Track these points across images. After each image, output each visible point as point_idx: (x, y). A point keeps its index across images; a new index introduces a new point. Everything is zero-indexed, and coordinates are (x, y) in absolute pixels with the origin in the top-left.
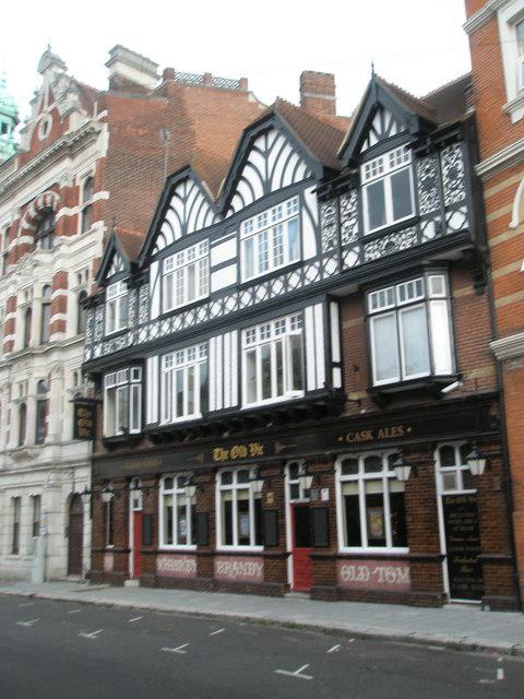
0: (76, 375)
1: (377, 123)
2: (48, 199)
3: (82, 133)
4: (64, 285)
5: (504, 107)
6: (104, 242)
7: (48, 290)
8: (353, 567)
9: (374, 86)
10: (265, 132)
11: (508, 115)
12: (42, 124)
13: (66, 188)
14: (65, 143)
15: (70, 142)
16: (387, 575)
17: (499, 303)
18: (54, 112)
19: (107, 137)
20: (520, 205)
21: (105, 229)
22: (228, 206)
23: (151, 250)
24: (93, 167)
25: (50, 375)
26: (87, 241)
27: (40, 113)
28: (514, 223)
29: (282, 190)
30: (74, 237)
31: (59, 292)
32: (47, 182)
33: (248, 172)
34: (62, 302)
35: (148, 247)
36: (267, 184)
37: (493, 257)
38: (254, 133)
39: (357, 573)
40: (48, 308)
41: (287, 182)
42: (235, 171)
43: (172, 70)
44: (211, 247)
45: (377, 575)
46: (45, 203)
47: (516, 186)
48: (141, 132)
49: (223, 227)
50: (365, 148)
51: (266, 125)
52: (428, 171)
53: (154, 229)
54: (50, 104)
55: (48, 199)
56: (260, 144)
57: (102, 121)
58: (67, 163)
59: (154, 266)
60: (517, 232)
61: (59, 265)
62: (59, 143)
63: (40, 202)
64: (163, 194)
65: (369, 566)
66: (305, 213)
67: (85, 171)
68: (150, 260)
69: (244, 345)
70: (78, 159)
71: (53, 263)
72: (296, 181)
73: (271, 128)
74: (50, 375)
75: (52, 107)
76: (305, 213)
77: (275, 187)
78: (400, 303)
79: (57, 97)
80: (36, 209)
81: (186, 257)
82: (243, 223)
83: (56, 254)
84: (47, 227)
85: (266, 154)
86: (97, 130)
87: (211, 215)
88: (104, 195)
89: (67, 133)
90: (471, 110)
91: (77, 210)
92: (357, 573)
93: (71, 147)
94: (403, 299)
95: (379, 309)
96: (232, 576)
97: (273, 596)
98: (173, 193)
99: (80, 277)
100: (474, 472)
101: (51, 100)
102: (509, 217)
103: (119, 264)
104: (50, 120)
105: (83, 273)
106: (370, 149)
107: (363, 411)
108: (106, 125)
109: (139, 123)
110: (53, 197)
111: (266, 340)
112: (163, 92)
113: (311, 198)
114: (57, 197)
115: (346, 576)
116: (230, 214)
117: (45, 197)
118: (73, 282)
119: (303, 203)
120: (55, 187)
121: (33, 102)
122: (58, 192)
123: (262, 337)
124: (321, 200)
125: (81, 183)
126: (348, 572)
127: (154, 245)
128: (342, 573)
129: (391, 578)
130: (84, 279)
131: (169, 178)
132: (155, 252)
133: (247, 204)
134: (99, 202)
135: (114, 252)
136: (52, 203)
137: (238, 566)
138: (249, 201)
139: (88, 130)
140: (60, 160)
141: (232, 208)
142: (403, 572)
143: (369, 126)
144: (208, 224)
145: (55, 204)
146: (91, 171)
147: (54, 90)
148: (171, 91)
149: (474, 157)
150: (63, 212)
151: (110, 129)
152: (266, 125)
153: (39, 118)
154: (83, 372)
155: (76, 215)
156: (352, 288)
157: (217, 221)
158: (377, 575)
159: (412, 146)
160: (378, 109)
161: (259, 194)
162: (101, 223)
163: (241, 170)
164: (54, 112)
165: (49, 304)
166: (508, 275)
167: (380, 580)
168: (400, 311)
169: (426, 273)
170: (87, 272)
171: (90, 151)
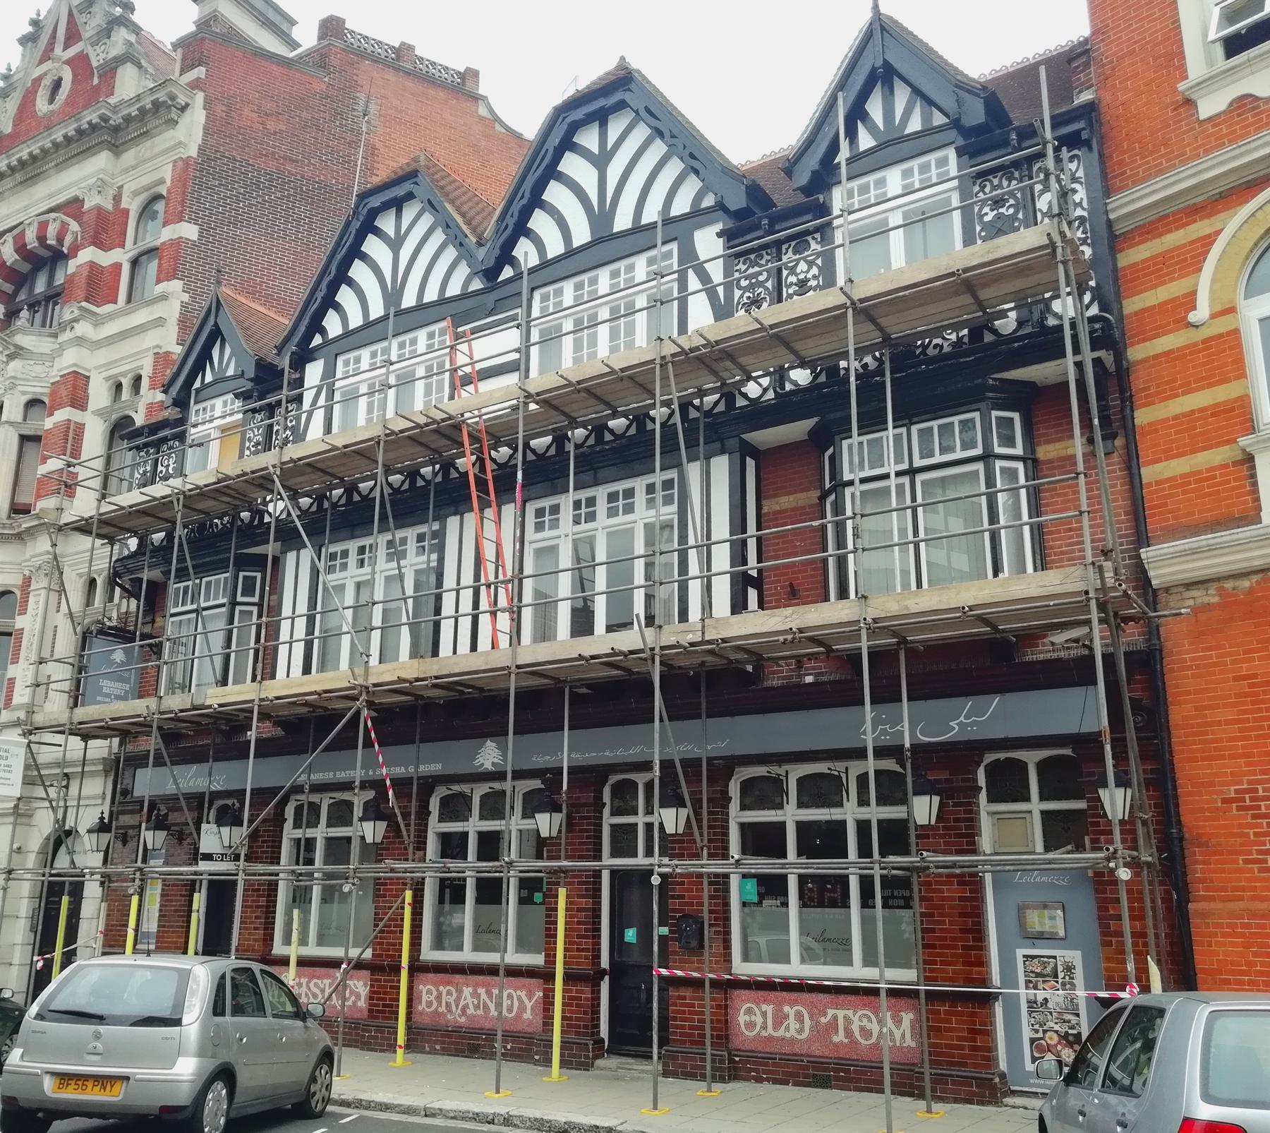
0: (92, 583)
1: (875, 108)
2: (52, 231)
3: (147, 102)
4: (79, 401)
5: (1182, 86)
6: (183, 322)
7: (35, 411)
8: (769, 1009)
9: (877, 27)
10: (397, 205)
11: (1189, 103)
12: (47, 82)
13: (99, 210)
14: (104, 119)
15: (116, 119)
16: (855, 1028)
17: (1149, 473)
18: (80, 64)
19: (203, 120)
20: (1214, 280)
21: (186, 297)
22: (506, 257)
23: (308, 337)
24: (167, 173)
25: (27, 581)
26: (141, 316)
27: (40, 63)
28: (1201, 313)
29: (420, 307)
30: (109, 308)
31: (62, 415)
32: (51, 196)
33: (555, 193)
34: (72, 438)
35: (302, 328)
36: (392, 295)
37: (1138, 381)
38: (375, 202)
39: (780, 1020)
40: (30, 448)
41: (431, 295)
42: (528, 186)
43: (341, 22)
44: (457, 337)
45: (833, 1025)
46: (42, 238)
47: (1207, 242)
48: (272, 125)
49: (491, 298)
50: (197, 384)
51: (400, 191)
52: (998, 203)
53: (320, 295)
54: (67, 46)
55: (52, 231)
56: (589, 139)
57: (196, 85)
58: (101, 161)
59: (314, 372)
60: (1206, 333)
61: (71, 359)
62: (91, 116)
63: (31, 238)
64: (348, 224)
65: (811, 1007)
66: (694, 282)
67: (146, 180)
68: (302, 358)
69: (530, 534)
70: (129, 157)
71: (53, 356)
72: (449, 294)
73: (410, 196)
74: (27, 581)
75: (71, 52)
76: (694, 282)
77: (409, 300)
78: (203, 605)
79: (88, 32)
80: (21, 248)
81: (421, 346)
82: (537, 295)
83: (66, 336)
84: (40, 287)
85: (395, 245)
86: (182, 100)
87: (463, 271)
88: (189, 231)
89: (112, 100)
90: (1086, 97)
91: (120, 256)
92: (780, 1020)
93: (117, 129)
94: (207, 599)
95: (180, 609)
96: (456, 1018)
97: (824, 1087)
98: (369, 227)
99: (119, 386)
100: (545, 833)
101: (73, 36)
102: (1189, 301)
103: (226, 361)
104: (67, 75)
105: (126, 382)
106: (204, 386)
107: (809, 679)
108: (200, 97)
109: (268, 106)
110: (64, 228)
111: (622, 518)
112: (319, 58)
113: (708, 242)
114: (74, 226)
115: (750, 1025)
116: (508, 272)
117: (43, 226)
118: (99, 395)
119: (688, 255)
120: (73, 207)
121: (25, 40)
122: (78, 217)
123: (577, 521)
124: (733, 258)
125: (133, 205)
126: (759, 1020)
127: (316, 326)
128: (742, 1019)
129: (866, 1033)
130: (126, 394)
131: (363, 196)
132: (317, 340)
133: (351, 327)
134: (178, 243)
135: (216, 334)
136: (60, 240)
137: (475, 995)
138: (355, 321)
139: (161, 96)
140: (87, 152)
141: (323, 331)
142: (898, 1022)
143: (857, 114)
144: (454, 289)
145: (68, 240)
146: (162, 181)
147: (81, 19)
148: (334, 60)
149: (1106, 184)
150: (87, 255)
151: (208, 105)
152: (400, 191)
153: (38, 72)
154: (112, 582)
155: (117, 267)
156: (798, 430)
157: (477, 285)
158: (833, 1025)
159: (244, 396)
160: (885, 76)
161: (582, 234)
162: (175, 286)
163: (346, 264)
164: (80, 64)
165: (36, 439)
166: (1176, 417)
167: (840, 1037)
168: (919, 478)
169: (837, 438)
170: (138, 379)
171: (165, 139)
